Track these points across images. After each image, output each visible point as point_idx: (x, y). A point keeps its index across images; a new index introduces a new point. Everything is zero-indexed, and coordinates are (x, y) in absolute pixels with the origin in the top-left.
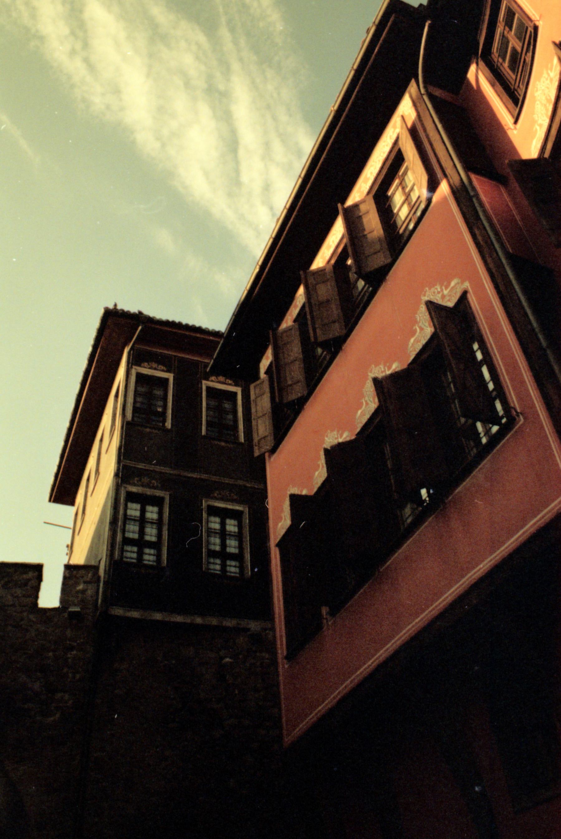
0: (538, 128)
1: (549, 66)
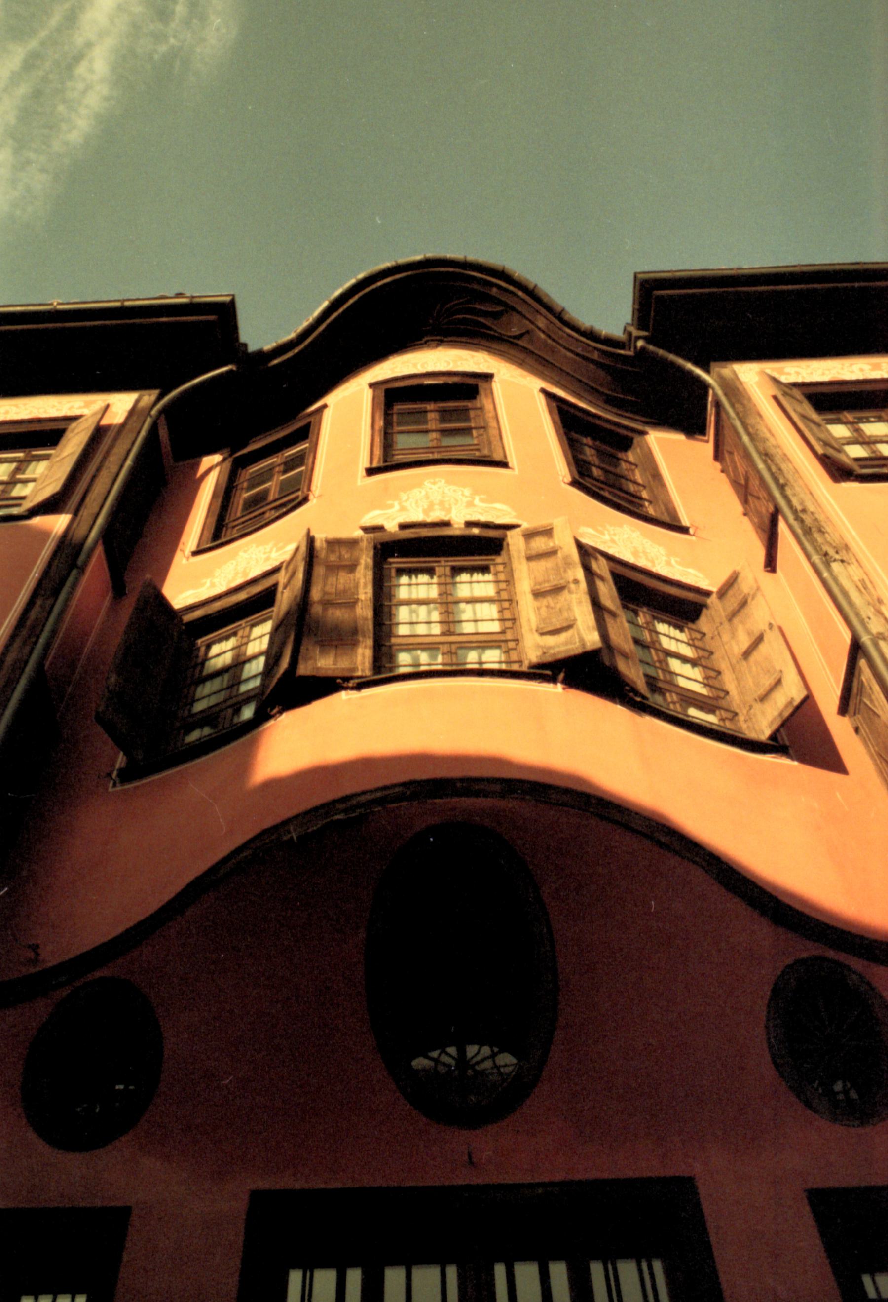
0: (208, 584)
1: (281, 545)
